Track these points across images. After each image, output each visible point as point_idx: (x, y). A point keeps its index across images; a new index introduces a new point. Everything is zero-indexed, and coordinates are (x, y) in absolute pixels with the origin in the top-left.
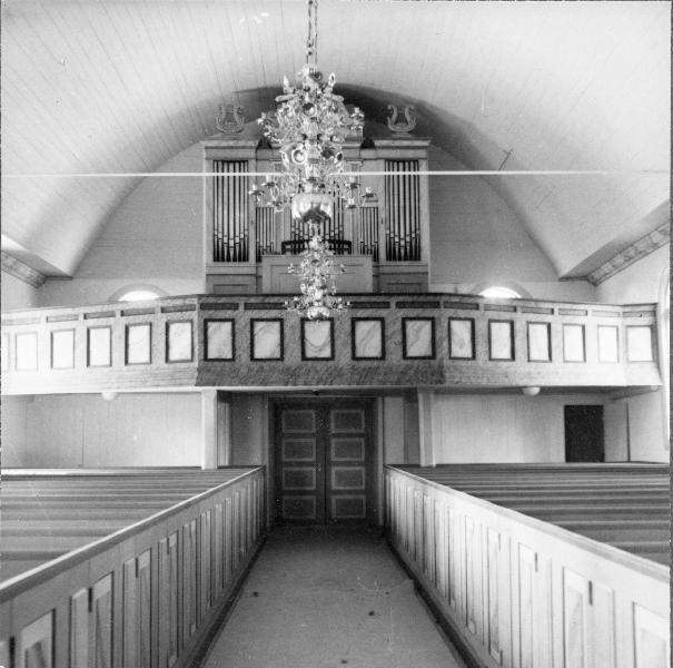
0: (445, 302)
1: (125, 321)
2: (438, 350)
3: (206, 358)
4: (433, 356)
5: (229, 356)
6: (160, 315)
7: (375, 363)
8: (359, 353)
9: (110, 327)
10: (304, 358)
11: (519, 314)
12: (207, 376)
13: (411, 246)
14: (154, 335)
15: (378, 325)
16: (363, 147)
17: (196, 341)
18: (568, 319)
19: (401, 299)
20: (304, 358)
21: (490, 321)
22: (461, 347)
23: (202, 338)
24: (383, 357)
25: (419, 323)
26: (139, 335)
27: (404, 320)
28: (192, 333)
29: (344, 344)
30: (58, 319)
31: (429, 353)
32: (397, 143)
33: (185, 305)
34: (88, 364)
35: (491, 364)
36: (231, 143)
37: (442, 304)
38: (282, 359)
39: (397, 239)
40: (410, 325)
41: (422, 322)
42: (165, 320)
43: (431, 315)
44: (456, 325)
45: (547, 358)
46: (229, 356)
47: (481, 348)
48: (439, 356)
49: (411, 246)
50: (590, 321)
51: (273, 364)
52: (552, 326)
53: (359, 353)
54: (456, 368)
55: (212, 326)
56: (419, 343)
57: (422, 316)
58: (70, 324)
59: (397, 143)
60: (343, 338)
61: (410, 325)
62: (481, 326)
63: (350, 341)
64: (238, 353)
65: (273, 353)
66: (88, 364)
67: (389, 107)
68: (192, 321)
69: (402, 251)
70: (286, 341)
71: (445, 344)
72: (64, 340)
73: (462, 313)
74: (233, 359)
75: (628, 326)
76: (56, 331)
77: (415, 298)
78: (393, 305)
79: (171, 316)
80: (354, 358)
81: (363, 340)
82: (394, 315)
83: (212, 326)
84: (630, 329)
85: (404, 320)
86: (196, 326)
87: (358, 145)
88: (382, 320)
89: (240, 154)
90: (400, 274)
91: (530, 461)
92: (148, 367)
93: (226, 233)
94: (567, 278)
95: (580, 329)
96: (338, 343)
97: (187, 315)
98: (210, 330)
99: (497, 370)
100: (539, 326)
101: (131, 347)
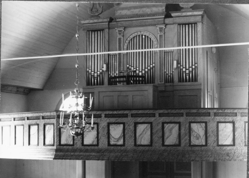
3: (60, 144)
5: (72, 143)
7: (147, 148)
8: (138, 143)
14: (39, 130)
17: (55, 134)
19: (134, 112)
21: (218, 122)
22: (198, 139)
23: (58, 133)
24: (151, 145)
25: (172, 125)
26: (34, 129)
27: (163, 123)
28: (54, 130)
31: (177, 143)
33: (50, 116)
35: (218, 148)
36: (96, 21)
38: (98, 145)
39: (184, 70)
40: (166, 126)
42: (43, 123)
43: (178, 121)
44: (194, 126)
47: (211, 140)
51: (93, 147)
53: (138, 143)
54: (194, 152)
56: (171, 139)
57: (173, 121)
59: (184, 14)
60: (129, 133)
61: (166, 126)
62: (212, 126)
63: (133, 135)
64: (75, 142)
65: (93, 142)
69: (187, 77)
70: (100, 135)
72: (20, 129)
78: (157, 115)
80: (135, 145)
81: (141, 135)
82: (158, 120)
85: (163, 123)
87: (164, 17)
88: (151, 123)
90: (185, 90)
93: (93, 70)
96: (127, 136)
101: (31, 136)
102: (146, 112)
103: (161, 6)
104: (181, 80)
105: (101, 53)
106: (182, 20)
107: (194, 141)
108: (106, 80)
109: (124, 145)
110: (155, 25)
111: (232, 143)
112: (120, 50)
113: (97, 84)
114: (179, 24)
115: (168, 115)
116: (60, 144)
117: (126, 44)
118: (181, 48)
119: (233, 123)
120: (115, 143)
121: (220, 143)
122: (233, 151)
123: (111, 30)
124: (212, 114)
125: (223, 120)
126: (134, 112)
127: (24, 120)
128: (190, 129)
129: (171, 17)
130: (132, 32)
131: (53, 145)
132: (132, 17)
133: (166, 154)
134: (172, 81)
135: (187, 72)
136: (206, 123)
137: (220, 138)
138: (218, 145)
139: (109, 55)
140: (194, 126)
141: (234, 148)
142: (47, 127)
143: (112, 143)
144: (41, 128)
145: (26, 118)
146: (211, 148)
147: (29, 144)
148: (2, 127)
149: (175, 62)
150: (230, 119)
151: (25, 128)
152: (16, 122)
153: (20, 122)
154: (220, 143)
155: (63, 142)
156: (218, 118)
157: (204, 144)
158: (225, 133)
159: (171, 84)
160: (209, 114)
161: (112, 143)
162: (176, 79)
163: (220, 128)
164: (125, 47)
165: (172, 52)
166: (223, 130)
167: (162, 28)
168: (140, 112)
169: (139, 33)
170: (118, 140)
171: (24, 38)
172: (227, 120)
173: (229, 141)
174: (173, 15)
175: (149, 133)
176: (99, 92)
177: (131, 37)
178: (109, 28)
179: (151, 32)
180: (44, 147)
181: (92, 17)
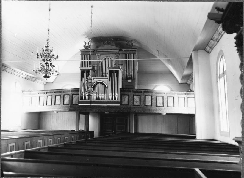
1: (55, 94)
2: (130, 103)
4: (129, 104)
9: (52, 96)
12: (72, 108)
13: (130, 76)
16: (120, 50)
17: (70, 99)
21: (145, 96)
23: (71, 99)
26: (58, 98)
29: (165, 99)
31: (128, 104)
32: (128, 50)
34: (47, 104)
35: (145, 107)
37: (131, 91)
41: (125, 96)
42: (63, 94)
44: (135, 97)
47: (142, 103)
49: (130, 76)
50: (176, 96)
52: (164, 97)
58: (43, 95)
59: (128, 50)
62: (142, 97)
66: (47, 104)
72: (42, 99)
73: (137, 94)
75: (188, 97)
76: (41, 96)
84: (188, 98)
86: (70, 96)
91: (167, 133)
92: (60, 106)
94: (180, 84)
95: (173, 98)
98: (73, 97)
99: (147, 109)
101: (56, 101)
107: (135, 103)
111: (151, 105)
112: (93, 59)
119: (152, 96)
121: (146, 105)
122: (151, 108)
123: (94, 56)
124: (143, 92)
125: (147, 95)
127: (53, 93)
131: (69, 104)
132: (104, 50)
133: (122, 109)
136: (140, 95)
137: (146, 102)
138: (145, 106)
140: (135, 97)
141: (152, 107)
142: (65, 96)
144: (54, 97)
145: (54, 92)
146: (142, 107)
148: (39, 97)
150: (150, 94)
151: (53, 97)
152: (48, 94)
153: (50, 94)
155: (74, 103)
156: (145, 94)
157: (139, 105)
158: (148, 101)
160: (141, 92)
163: (146, 98)
166: (147, 99)
167: (118, 55)
169: (107, 57)
172: (149, 95)
176: (168, 97)
178: (93, 54)
180: (63, 105)
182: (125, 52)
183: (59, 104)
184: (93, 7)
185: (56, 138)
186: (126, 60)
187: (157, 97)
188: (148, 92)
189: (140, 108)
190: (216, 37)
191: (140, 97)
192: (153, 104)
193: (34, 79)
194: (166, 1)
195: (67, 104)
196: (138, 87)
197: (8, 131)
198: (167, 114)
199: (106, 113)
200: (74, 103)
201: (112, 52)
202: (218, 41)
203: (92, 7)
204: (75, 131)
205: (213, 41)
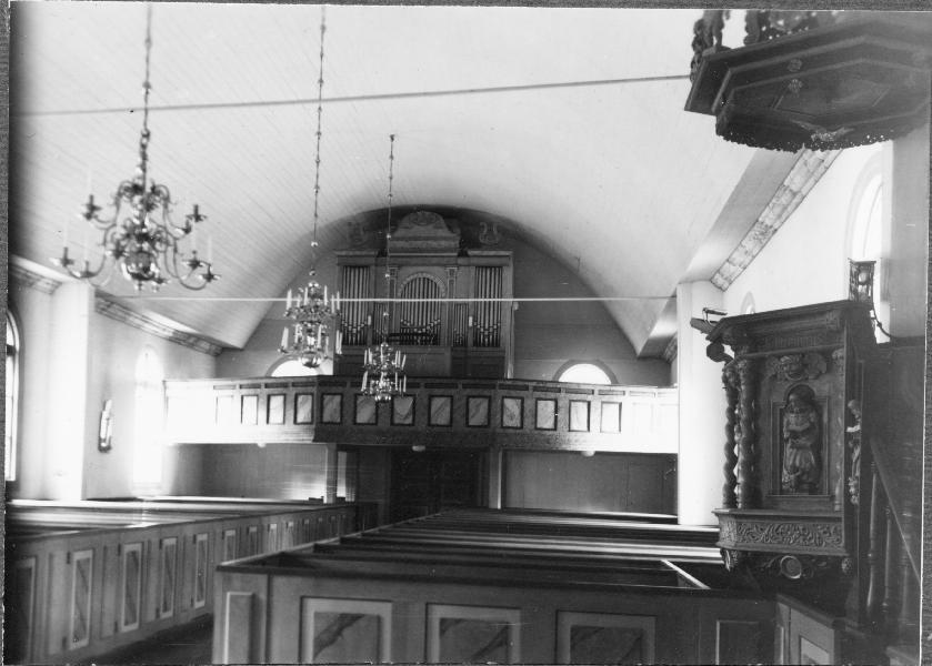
0: (501, 385)
2: (492, 421)
6: (291, 388)
8: (433, 422)
10: (392, 423)
11: (563, 394)
15: (449, 400)
16: (460, 255)
18: (606, 398)
19: (429, 381)
20: (392, 423)
25: (479, 400)
30: (221, 388)
32: (485, 253)
35: (536, 432)
36: (358, 253)
38: (376, 424)
40: (472, 401)
41: (481, 400)
44: (509, 403)
45: (586, 428)
46: (339, 420)
48: (492, 426)
52: (592, 404)
53: (433, 422)
55: (327, 398)
56: (478, 416)
59: (485, 253)
61: (472, 401)
62: (529, 403)
67: (481, 224)
68: (312, 394)
71: (499, 416)
73: (513, 393)
74: (341, 423)
77: (477, 381)
79: (300, 389)
80: (429, 424)
82: (460, 393)
83: (327, 398)
87: (456, 254)
89: (362, 261)
95: (617, 406)
97: (310, 389)
98: (325, 402)
100: (581, 403)
102: (445, 381)
103: (454, 240)
104: (476, 343)
105: (364, 300)
106: (483, 262)
107: (508, 422)
108: (369, 339)
109: (413, 425)
110: (445, 266)
112: (391, 297)
113: (356, 343)
114: (478, 267)
115: (475, 386)
116: (322, 422)
117: (400, 290)
118: (479, 300)
119: (556, 401)
120: (401, 422)
121: (539, 426)
126: (429, 381)
128: (502, 405)
129: (467, 255)
130: (410, 273)
134: (465, 343)
135: (486, 333)
138: (536, 428)
139: (375, 303)
140: (509, 403)
142: (300, 399)
143: (397, 421)
144: (291, 398)
147: (268, 422)
149: (471, 319)
150: (552, 395)
152: (244, 391)
153: (252, 391)
154: (539, 426)
155: (326, 418)
156: (538, 394)
159: (463, 349)
160: (527, 388)
161: (397, 421)
162: (470, 341)
163: (539, 407)
164: (399, 294)
165: (466, 304)
168: (438, 381)
169: (420, 275)
170: (406, 417)
171: (355, 213)
173: (549, 424)
174: (470, 253)
175: (448, 409)
177: (408, 279)
179: (437, 274)
181: (353, 247)
182: (475, 261)
183: (281, 420)
184: (395, 139)
185: (219, 531)
186: (496, 300)
187: (573, 404)
188: (548, 390)
189: (523, 435)
190: (738, 257)
191: (523, 403)
192: (560, 425)
193: (191, 341)
194: (590, 5)
195: (306, 421)
196: (515, 373)
197: (141, 500)
198: (597, 453)
199: (415, 448)
200: (326, 418)
201: (435, 260)
202: (745, 268)
203: (392, 138)
204: (325, 501)
205: (732, 267)
